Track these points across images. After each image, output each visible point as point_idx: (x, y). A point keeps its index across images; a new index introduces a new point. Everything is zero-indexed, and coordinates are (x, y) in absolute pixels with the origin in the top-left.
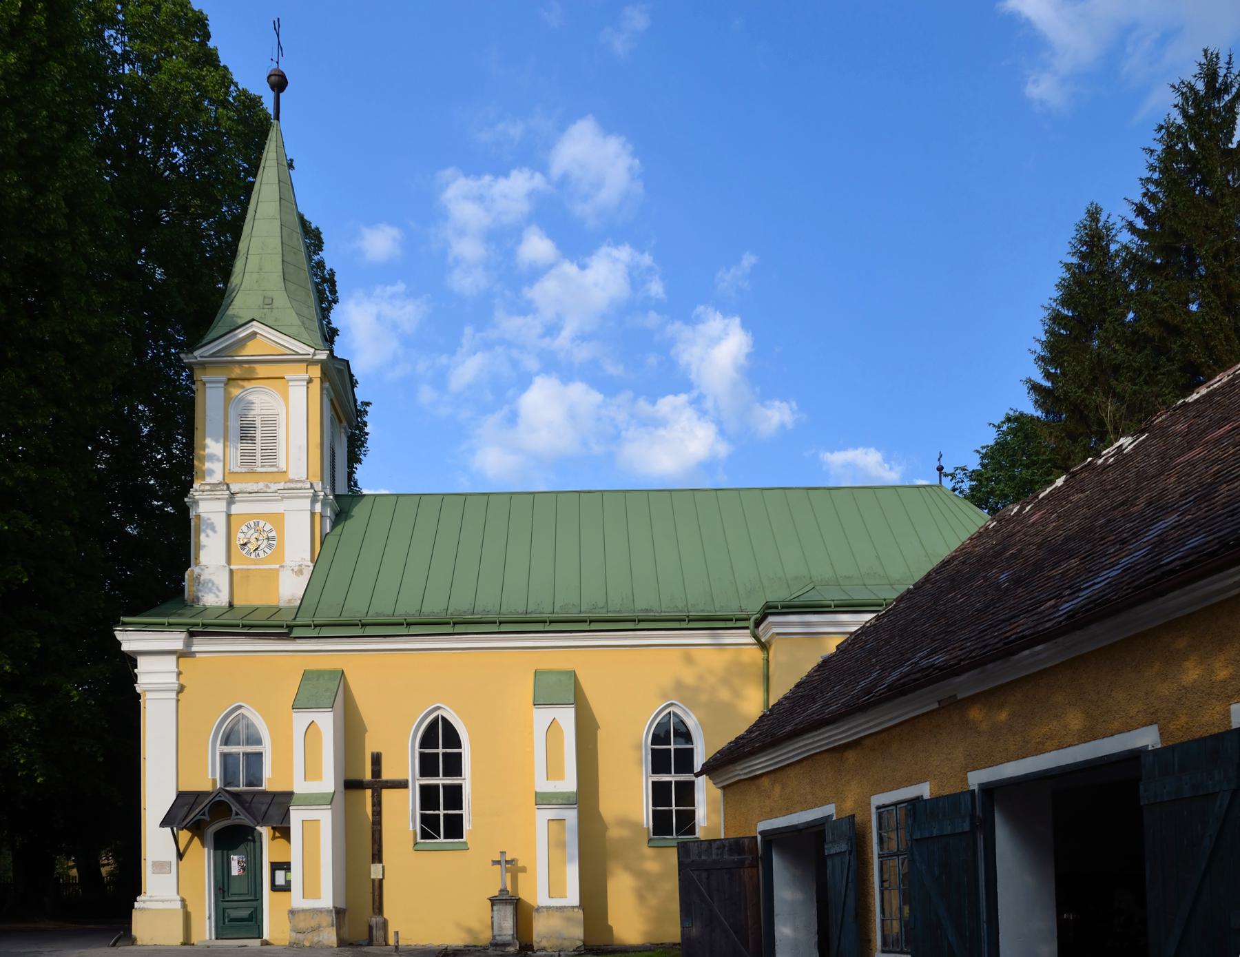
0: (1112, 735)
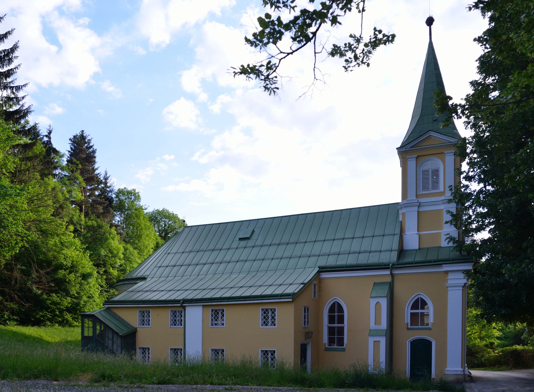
0: (203, 320)
